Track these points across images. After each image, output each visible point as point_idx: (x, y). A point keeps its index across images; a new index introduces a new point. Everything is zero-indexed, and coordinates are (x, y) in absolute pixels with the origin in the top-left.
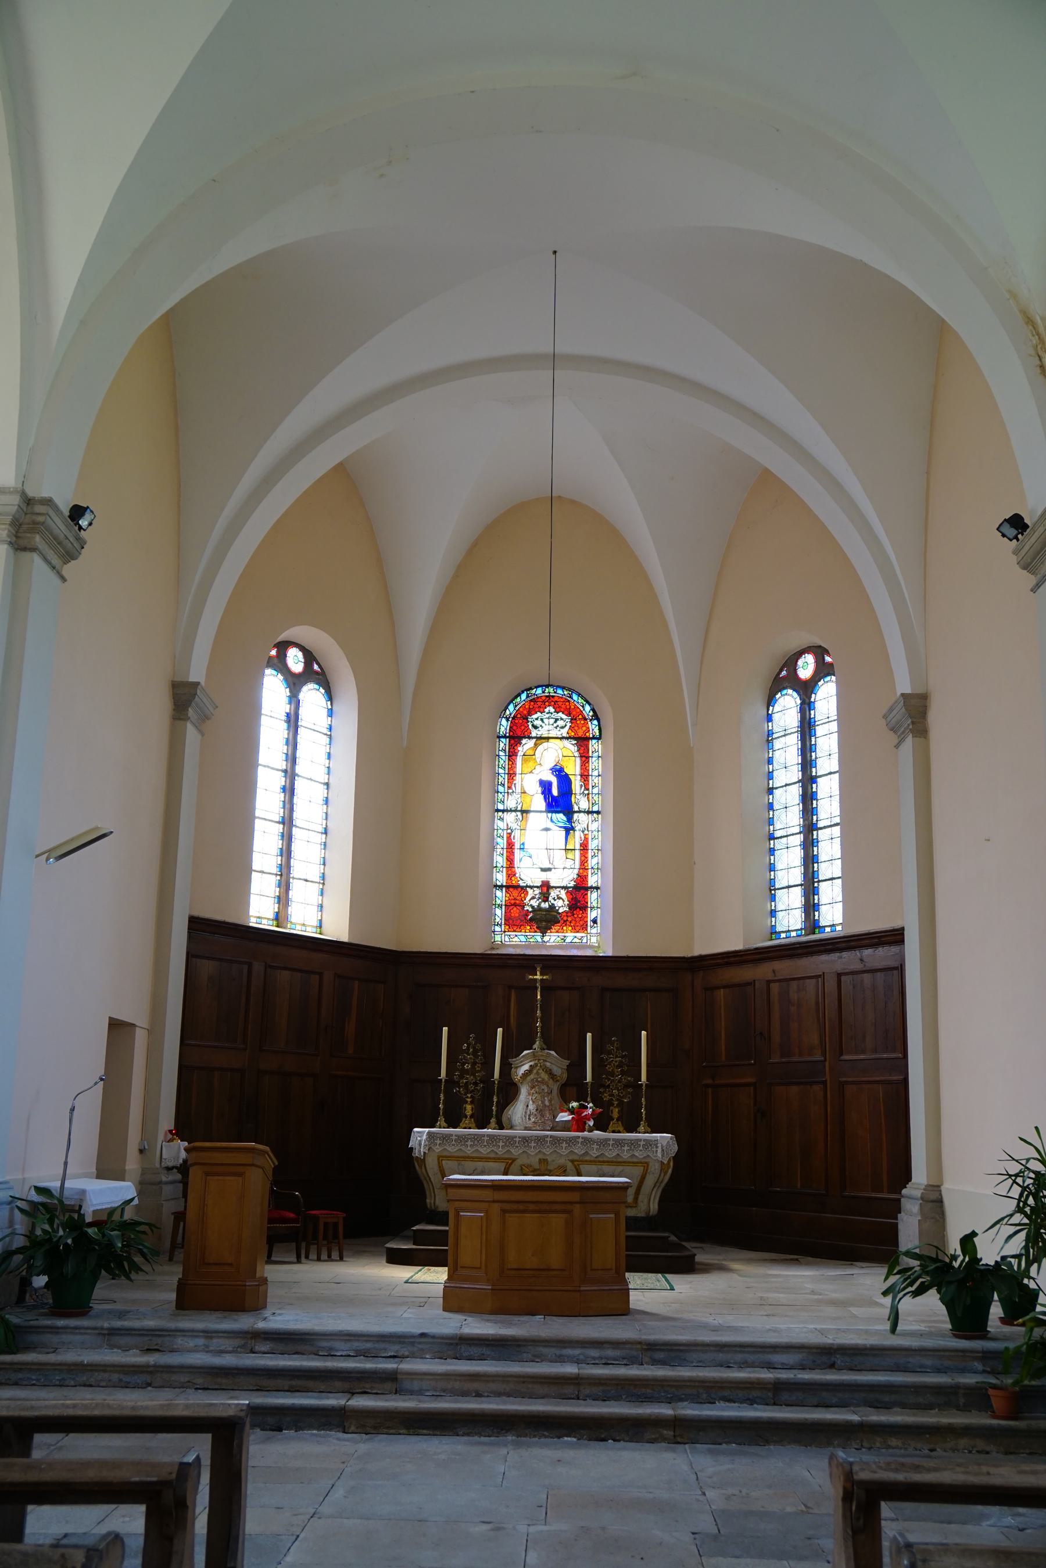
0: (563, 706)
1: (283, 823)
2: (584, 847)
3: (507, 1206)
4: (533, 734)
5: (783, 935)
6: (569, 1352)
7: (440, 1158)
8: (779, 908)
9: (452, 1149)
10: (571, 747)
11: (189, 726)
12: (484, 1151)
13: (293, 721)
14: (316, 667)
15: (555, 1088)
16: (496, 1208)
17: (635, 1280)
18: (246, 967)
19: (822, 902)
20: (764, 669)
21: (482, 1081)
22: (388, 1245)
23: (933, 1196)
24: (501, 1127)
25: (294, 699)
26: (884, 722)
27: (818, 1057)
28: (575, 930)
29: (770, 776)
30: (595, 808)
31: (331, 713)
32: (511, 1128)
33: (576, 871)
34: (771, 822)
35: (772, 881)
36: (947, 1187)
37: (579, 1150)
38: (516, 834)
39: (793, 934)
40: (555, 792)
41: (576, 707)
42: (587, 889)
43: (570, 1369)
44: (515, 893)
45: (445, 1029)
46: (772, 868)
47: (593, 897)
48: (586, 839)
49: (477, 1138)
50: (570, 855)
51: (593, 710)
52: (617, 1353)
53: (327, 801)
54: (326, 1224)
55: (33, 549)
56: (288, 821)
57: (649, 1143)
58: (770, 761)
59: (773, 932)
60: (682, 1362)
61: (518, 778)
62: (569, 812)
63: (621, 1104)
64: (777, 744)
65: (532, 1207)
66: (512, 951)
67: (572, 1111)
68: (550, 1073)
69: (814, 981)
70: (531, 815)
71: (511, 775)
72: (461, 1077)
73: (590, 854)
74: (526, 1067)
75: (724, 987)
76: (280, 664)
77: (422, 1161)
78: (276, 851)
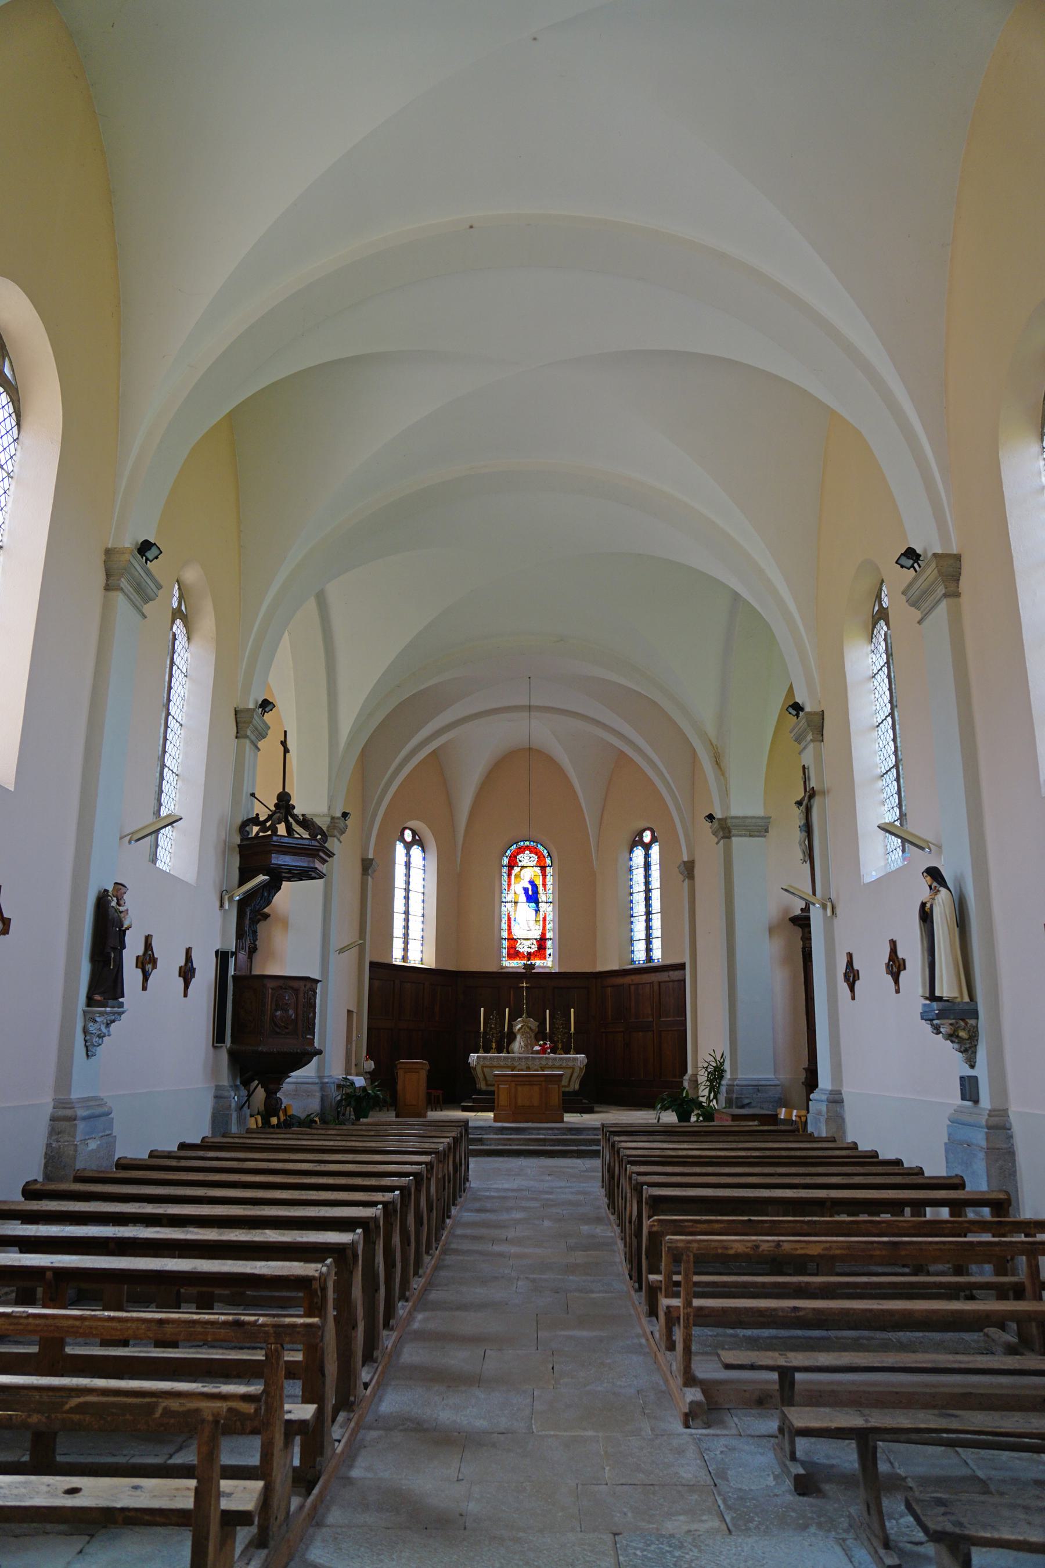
0: (534, 851)
1: (405, 913)
2: (544, 919)
3: (517, 1083)
4: (520, 865)
5: (637, 963)
6: (541, 1132)
7: (482, 1067)
8: (635, 949)
9: (488, 1063)
10: (538, 870)
11: (369, 877)
12: (502, 1064)
13: (408, 865)
14: (417, 837)
15: (533, 1035)
16: (513, 1084)
17: (565, 1115)
18: (392, 983)
19: (654, 948)
20: (627, 837)
21: (500, 1032)
22: (462, 1104)
23: (694, 1079)
24: (509, 1053)
25: (408, 855)
26: (678, 870)
27: (651, 1019)
28: (540, 959)
29: (631, 887)
30: (550, 900)
31: (424, 859)
32: (513, 1053)
33: (541, 931)
34: (631, 909)
35: (632, 938)
36: (846, 1090)
37: (544, 1062)
38: (512, 913)
39: (641, 962)
40: (530, 893)
41: (540, 851)
42: (546, 939)
43: (541, 1137)
44: (512, 942)
45: (482, 1009)
46: (632, 930)
47: (549, 944)
48: (545, 916)
49: (498, 1058)
50: (538, 924)
51: (548, 852)
52: (558, 1132)
53: (423, 901)
54: (434, 1096)
55: (334, 836)
56: (407, 913)
57: (574, 1059)
58: (631, 880)
59: (633, 961)
60: (581, 1134)
61: (512, 886)
62: (537, 903)
63: (562, 1042)
64: (635, 872)
65: (527, 1083)
66: (511, 970)
67: (540, 1045)
68: (530, 1028)
69: (649, 985)
70: (519, 904)
71: (509, 885)
72: (490, 1031)
73: (547, 922)
74: (519, 1026)
75: (611, 986)
76: (402, 839)
77: (475, 1069)
78: (402, 927)
